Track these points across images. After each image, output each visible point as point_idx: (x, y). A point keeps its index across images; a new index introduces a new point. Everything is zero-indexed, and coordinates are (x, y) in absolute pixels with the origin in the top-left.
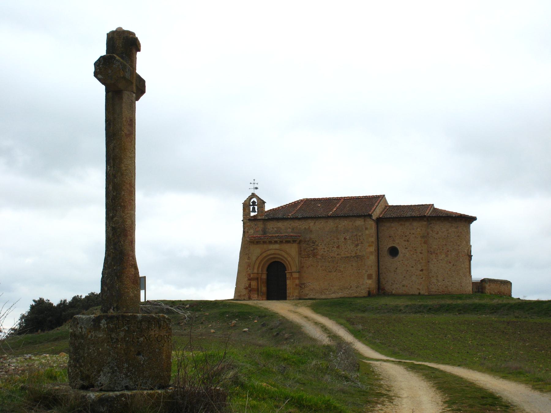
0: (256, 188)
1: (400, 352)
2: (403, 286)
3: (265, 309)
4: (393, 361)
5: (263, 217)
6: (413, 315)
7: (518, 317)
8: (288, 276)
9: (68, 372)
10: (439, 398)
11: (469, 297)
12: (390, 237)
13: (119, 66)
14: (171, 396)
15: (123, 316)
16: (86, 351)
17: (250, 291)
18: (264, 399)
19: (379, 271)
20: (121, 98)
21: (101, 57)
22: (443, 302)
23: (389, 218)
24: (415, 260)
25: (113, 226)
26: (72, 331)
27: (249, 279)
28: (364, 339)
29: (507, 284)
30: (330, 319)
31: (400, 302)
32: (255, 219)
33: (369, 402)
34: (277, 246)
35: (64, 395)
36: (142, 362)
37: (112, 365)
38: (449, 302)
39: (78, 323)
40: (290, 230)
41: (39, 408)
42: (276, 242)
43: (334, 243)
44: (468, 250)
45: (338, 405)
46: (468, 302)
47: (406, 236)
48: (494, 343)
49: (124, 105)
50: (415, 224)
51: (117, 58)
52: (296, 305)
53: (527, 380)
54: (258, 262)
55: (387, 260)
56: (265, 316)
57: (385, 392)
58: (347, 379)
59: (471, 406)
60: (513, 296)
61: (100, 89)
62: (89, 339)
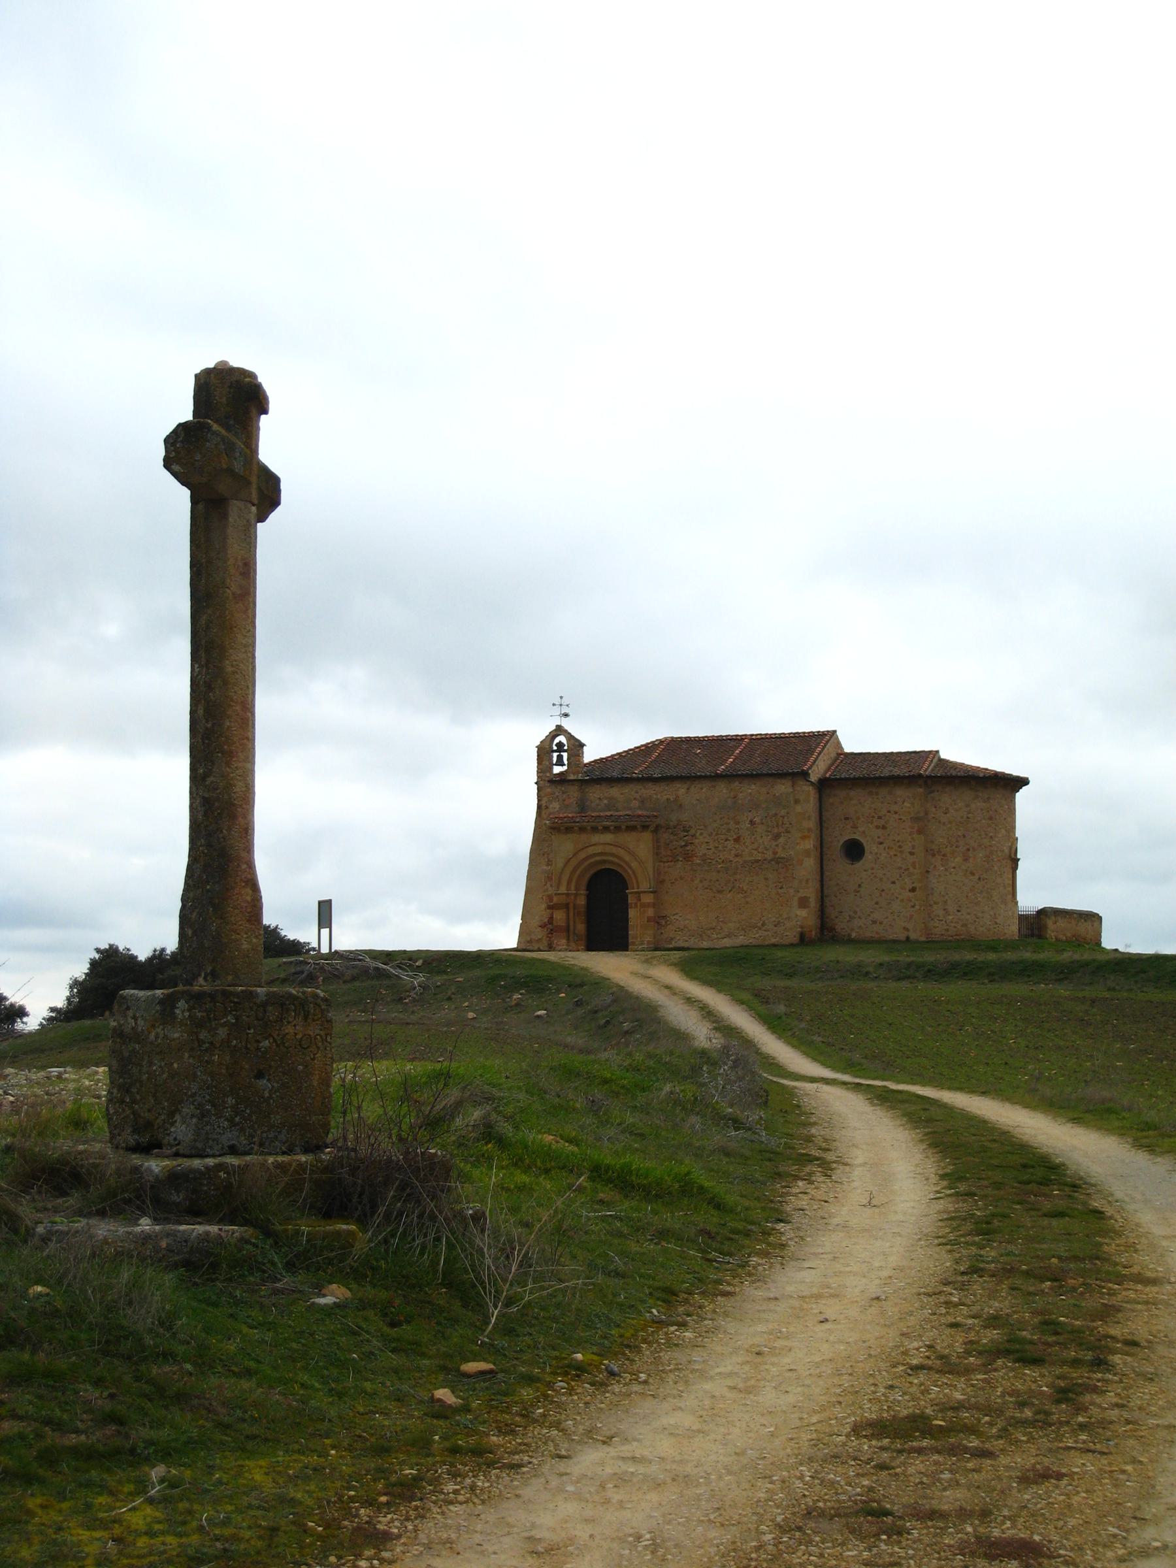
0: (566, 715)
1: (864, 1061)
2: (874, 922)
3: (582, 969)
4: (844, 1083)
5: (580, 777)
6: (893, 985)
7: (1114, 989)
8: (631, 900)
9: (108, 1114)
10: (931, 1166)
11: (1010, 945)
12: (846, 819)
13: (219, 447)
14: (328, 1169)
15: (224, 993)
16: (145, 1069)
17: (551, 932)
18: (547, 1171)
19: (822, 891)
20: (224, 516)
21: (180, 425)
22: (956, 957)
23: (846, 779)
24: (900, 868)
25: (206, 795)
26: (115, 1024)
27: (549, 907)
28: (790, 1033)
29: (1093, 919)
30: (719, 991)
31: (869, 957)
32: (562, 779)
33: (779, 1175)
34: (608, 837)
35: (95, 1166)
36: (267, 1095)
37: (199, 1099)
38: (969, 956)
39: (128, 1008)
40: (635, 804)
41: (40, 1192)
42: (606, 829)
43: (729, 830)
44: (1011, 848)
45: (706, 1184)
46: (1010, 956)
47: (880, 818)
48: (1062, 1043)
49: (230, 530)
50: (900, 792)
51: (215, 427)
52: (647, 961)
53: (1123, 1128)
55: (840, 867)
56: (581, 985)
57: (815, 1153)
58: (737, 1124)
59: (997, 1185)
60: (1103, 945)
61: (180, 497)
62: (151, 1043)
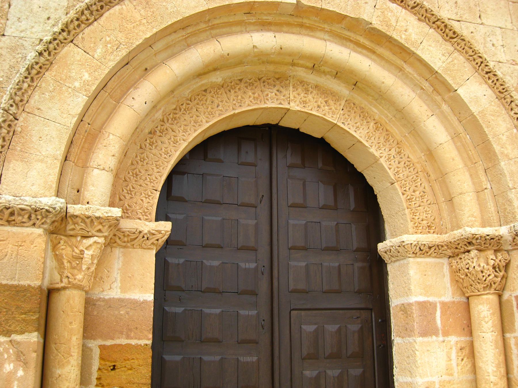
54: (83, 69)
